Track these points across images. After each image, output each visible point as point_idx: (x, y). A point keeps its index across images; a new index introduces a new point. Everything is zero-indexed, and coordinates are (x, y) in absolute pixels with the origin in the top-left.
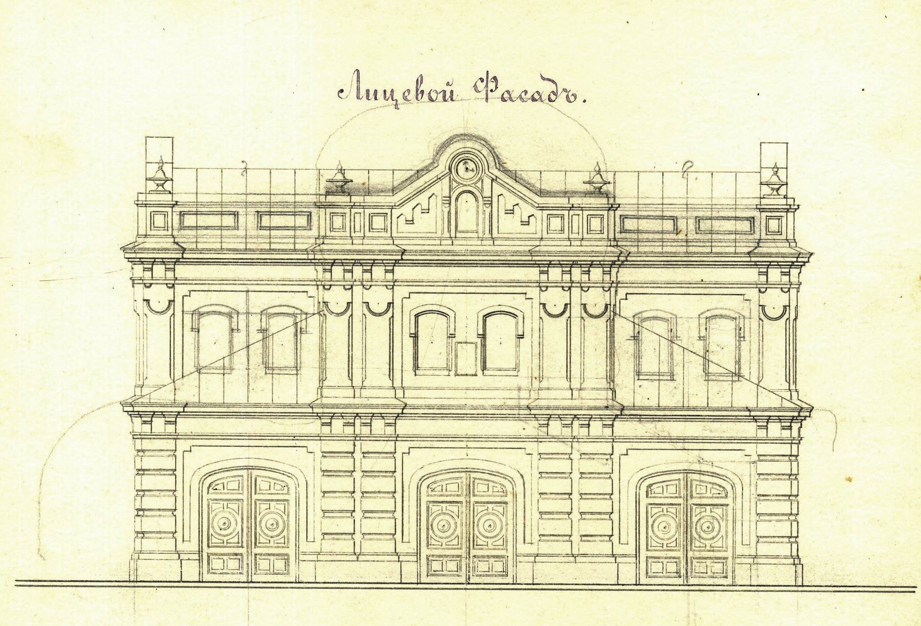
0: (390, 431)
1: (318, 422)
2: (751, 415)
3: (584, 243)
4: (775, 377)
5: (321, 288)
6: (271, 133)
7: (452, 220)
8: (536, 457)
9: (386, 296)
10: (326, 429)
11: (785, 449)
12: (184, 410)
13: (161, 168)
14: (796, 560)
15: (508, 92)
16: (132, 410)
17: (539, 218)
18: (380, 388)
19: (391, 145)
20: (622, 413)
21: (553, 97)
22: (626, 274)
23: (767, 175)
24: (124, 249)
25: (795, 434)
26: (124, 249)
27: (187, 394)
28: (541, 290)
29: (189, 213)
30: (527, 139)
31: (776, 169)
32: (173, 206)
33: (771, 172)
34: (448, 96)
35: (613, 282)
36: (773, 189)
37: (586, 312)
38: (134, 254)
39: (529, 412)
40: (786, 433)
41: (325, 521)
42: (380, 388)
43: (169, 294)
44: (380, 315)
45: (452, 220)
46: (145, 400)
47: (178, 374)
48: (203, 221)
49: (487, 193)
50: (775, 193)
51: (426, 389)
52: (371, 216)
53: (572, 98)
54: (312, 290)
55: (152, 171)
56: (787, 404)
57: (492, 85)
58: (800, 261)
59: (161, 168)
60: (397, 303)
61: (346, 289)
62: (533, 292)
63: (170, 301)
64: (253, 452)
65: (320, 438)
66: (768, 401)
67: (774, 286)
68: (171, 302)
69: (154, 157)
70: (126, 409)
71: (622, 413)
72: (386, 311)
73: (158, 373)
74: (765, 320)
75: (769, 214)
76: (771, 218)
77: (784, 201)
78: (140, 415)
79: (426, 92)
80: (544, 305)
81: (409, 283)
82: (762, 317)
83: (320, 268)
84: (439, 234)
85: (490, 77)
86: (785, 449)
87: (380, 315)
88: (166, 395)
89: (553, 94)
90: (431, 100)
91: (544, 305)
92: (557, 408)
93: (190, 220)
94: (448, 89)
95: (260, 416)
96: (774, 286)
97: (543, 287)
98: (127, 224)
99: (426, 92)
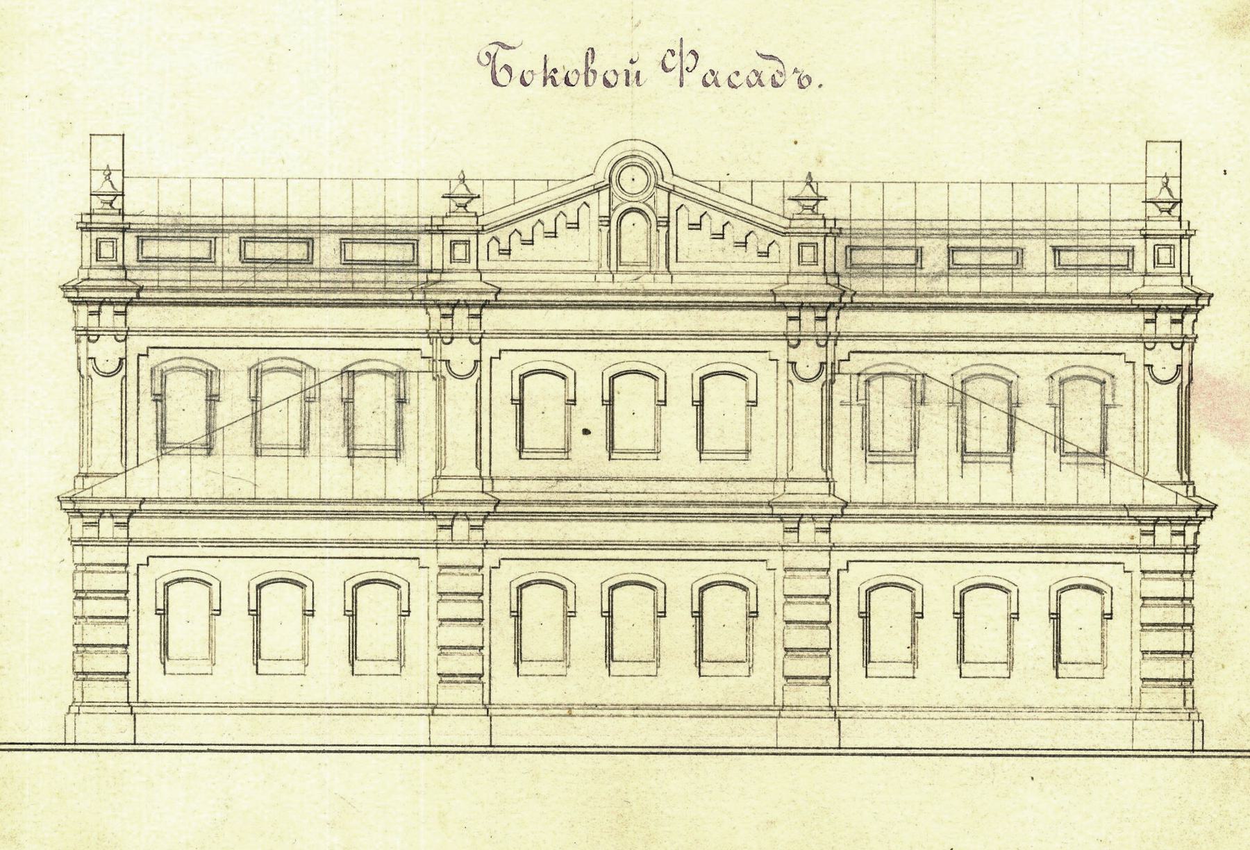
0: (476, 535)
1: (433, 524)
2: (1128, 514)
3: (792, 279)
4: (1164, 463)
5: (84, 339)
6: (357, 135)
7: (614, 249)
8: (1137, 575)
9: (472, 352)
10: (444, 535)
11: (1175, 562)
12: (137, 509)
13: (1166, 185)
14: (1191, 711)
15: (713, 72)
16: (73, 507)
17: (785, 248)
18: (812, 480)
19: (534, 147)
20: (844, 511)
21: (779, 80)
22: (851, 321)
23: (1155, 190)
24: (64, 288)
25: (1189, 540)
26: (64, 288)
27: (142, 484)
28: (789, 345)
29: (1068, 249)
30: (706, 139)
31: (108, 173)
32: (478, 232)
33: (1159, 183)
34: (633, 78)
35: (1186, 336)
36: (104, 202)
37: (795, 372)
38: (77, 295)
39: (772, 512)
40: (1178, 540)
41: (789, 662)
42: (812, 480)
43: (473, 352)
44: (1167, 382)
45: (614, 249)
46: (87, 494)
47: (132, 461)
48: (1103, 258)
49: (662, 211)
50: (107, 206)
51: (858, 482)
52: (99, 242)
53: (805, 82)
54: (424, 344)
55: (99, 183)
56: (1182, 501)
57: (689, 61)
58: (1195, 302)
59: (1166, 185)
60: (132, 360)
61: (820, 346)
62: (1134, 351)
63: (821, 364)
64: (1084, 569)
65: (437, 545)
66: (1157, 496)
67: (807, 337)
68: (122, 362)
69: (100, 163)
70: (66, 506)
71: (496, 510)
72: (471, 374)
73: (106, 456)
74: (796, 382)
75: (1157, 241)
76: (457, 242)
77: (118, 219)
78: (80, 513)
79: (600, 73)
80: (794, 363)
81: (502, 335)
82: (792, 377)
83: (435, 312)
84: (594, 267)
85: (686, 50)
86: (1175, 562)
87: (1167, 382)
88: (114, 488)
89: (769, 74)
90: (606, 83)
91: (794, 363)
92: (463, 502)
93: (1120, 258)
94: (633, 69)
95: (1059, 520)
96: (807, 337)
97: (794, 340)
98: (68, 256)
99: (600, 73)
